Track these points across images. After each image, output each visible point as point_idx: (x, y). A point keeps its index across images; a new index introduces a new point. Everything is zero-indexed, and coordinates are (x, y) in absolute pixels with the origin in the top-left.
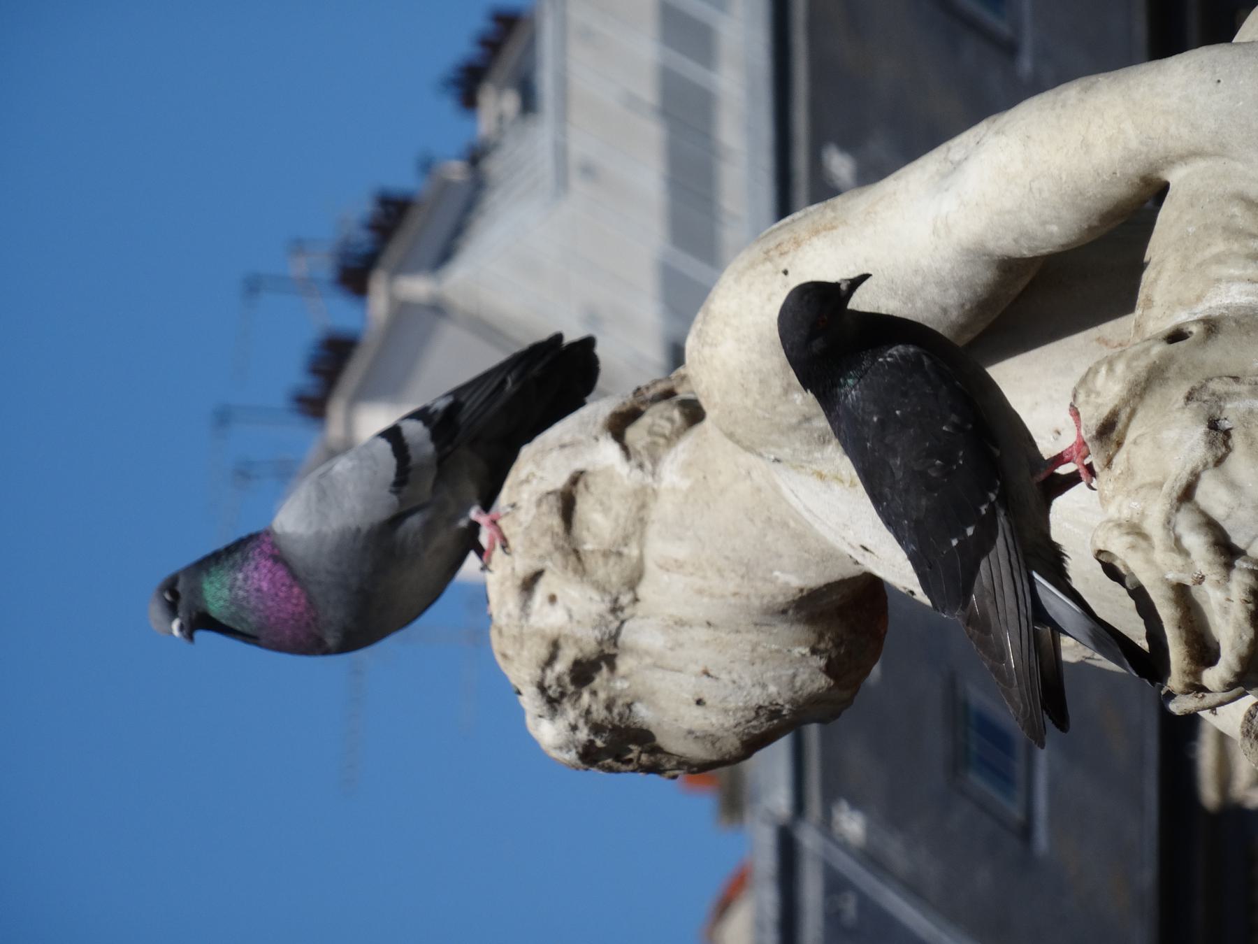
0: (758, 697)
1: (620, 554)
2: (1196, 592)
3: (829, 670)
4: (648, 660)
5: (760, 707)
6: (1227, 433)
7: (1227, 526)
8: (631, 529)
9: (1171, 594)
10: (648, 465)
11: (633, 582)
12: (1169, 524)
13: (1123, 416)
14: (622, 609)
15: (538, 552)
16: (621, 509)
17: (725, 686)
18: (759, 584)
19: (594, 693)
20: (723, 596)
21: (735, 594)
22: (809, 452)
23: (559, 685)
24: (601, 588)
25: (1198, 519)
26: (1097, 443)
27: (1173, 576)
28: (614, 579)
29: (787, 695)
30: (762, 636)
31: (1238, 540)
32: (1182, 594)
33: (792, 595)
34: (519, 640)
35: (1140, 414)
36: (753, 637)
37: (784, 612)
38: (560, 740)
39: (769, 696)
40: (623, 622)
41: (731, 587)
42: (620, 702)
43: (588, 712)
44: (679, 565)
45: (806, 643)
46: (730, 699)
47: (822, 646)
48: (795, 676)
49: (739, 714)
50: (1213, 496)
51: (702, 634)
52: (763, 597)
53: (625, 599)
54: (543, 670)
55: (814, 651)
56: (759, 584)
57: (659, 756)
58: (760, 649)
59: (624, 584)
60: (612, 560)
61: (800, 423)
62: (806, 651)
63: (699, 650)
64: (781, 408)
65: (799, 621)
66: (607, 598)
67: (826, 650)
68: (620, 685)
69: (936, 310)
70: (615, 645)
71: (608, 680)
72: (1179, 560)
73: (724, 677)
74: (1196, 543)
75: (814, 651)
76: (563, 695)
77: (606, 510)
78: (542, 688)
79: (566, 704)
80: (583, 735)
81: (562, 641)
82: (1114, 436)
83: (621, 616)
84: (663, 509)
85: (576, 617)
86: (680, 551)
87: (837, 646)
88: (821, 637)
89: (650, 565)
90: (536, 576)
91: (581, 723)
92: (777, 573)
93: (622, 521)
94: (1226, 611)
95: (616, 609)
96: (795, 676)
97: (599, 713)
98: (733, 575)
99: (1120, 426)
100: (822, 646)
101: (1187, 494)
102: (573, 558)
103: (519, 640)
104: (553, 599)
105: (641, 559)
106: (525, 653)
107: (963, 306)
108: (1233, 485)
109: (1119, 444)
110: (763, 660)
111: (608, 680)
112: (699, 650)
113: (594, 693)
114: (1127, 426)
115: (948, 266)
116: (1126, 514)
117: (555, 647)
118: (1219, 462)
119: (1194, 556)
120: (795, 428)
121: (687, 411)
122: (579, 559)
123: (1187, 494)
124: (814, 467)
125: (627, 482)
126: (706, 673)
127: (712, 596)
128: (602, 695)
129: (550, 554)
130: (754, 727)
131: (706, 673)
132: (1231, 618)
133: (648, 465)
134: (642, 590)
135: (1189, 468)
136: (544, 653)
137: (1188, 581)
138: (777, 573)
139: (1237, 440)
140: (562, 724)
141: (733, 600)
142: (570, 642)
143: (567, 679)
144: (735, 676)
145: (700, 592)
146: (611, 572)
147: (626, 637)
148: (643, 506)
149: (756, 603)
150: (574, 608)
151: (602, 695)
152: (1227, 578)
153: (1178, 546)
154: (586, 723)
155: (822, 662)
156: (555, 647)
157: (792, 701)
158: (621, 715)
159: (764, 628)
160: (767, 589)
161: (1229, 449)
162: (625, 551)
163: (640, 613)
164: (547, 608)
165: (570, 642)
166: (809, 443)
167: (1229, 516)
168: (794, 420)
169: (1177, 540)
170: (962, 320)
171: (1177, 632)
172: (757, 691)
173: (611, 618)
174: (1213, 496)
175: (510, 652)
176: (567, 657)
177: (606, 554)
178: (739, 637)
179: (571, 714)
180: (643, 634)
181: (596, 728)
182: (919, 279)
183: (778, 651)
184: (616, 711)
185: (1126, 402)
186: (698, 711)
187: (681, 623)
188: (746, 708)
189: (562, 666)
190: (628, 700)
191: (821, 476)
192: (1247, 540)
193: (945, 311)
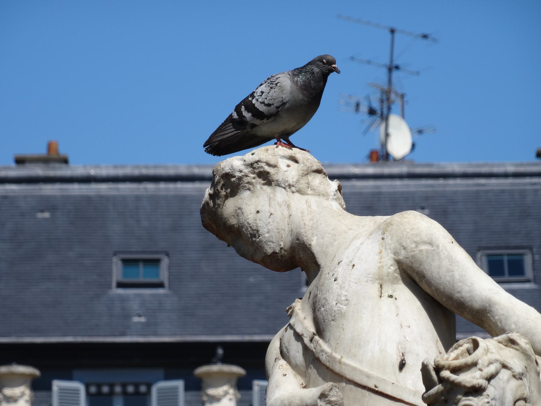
0: (263, 230)
1: (308, 188)
2: (474, 369)
3: (274, 253)
4: (272, 196)
5: (258, 231)
6: (521, 379)
7: (496, 378)
8: (317, 191)
9: (475, 361)
10: (335, 197)
11: (299, 191)
12: (497, 361)
13: (517, 347)
14: (290, 188)
15: (305, 161)
16: (322, 188)
17: (267, 220)
18: (310, 231)
19: (254, 178)
20: (303, 220)
21: (305, 224)
22: (390, 249)
23: (258, 167)
24: (298, 181)
25: (499, 369)
26: (507, 339)
27: (480, 362)
28: (301, 186)
29: (264, 240)
30: (287, 232)
31: (492, 382)
32: (474, 364)
33: (307, 242)
34: (274, 155)
35: (517, 352)
36: (287, 229)
37: (298, 239)
38: (235, 167)
39: (264, 234)
40: (285, 188)
41: (307, 223)
42: (250, 186)
43: (247, 176)
44: (310, 206)
45: (284, 246)
46: (261, 222)
47: (283, 251)
48: (273, 242)
49: (255, 225)
50: (504, 374)
51: (286, 213)
52: (305, 233)
53: (293, 189)
54: (265, 162)
55: (281, 248)
56: (310, 231)
57: (224, 198)
58: (283, 232)
59: (299, 189)
60: (307, 185)
61: (403, 246)
62: (282, 246)
63: (280, 213)
64: (408, 240)
65: (292, 244)
66: (294, 183)
67: (281, 252)
68: (258, 187)
69: (459, 290)
70: (276, 185)
71: (260, 183)
72: (486, 364)
73: (271, 220)
74: (492, 369)
75: (281, 248)
76: (254, 168)
77: (320, 183)
78: (257, 162)
79: (250, 169)
80: (238, 174)
81: (276, 168)
82: (509, 344)
83: (287, 188)
84: (325, 203)
85: (285, 173)
86: (314, 207)
87: (282, 256)
88: (285, 251)
89: (306, 197)
90: (296, 161)
91: (243, 174)
92: (316, 237)
93: (318, 188)
94: (474, 378)
95: (290, 186)
96: (273, 242)
97: (246, 180)
98: (312, 223)
99: (513, 346)
100: (283, 251)
101: (504, 366)
102: (306, 173)
103: (274, 155)
104: (288, 166)
105: (308, 194)
106: (271, 157)
107: (462, 298)
108: (508, 380)
109: (506, 346)
110: (279, 232)
111: (260, 183)
112: (280, 213)
113: (254, 178)
114: (513, 348)
115: (479, 294)
116: (490, 347)
117: (275, 166)
118: (514, 376)
119: (488, 368)
120: (401, 245)
121: (427, 211)
122: (306, 175)
123: (504, 366)
124: (384, 250)
125: (329, 190)
126: (271, 214)
127: (302, 217)
128: (253, 181)
129: (306, 165)
130: (247, 229)
131: (271, 214)
132: (472, 379)
133: (335, 197)
134: (297, 195)
135: (512, 367)
136: (272, 162)
137: (478, 366)
138: (316, 237)
139: (520, 382)
140: (242, 168)
141: (302, 223)
142: (277, 171)
143: (261, 170)
144: (272, 223)
145: (302, 213)
146: (302, 185)
147: (278, 189)
148: (324, 195)
149: (303, 230)
150: (288, 173)
151: (253, 181)
152: (483, 378)
153: (490, 363)
154: (243, 175)
155: (277, 251)
156: (275, 166)
157: (261, 241)
158: (245, 186)
159: (290, 233)
160: (309, 234)
161: (517, 379)
162: (309, 189)
163: (288, 193)
164: (286, 164)
165: (277, 171)
166: (394, 249)
167: (499, 379)
168: (404, 244)
169: (492, 363)
170: (455, 297)
171: (464, 363)
172: (266, 230)
173: (286, 184)
174: (504, 374)
175: (269, 152)
176: (271, 170)
177: (308, 183)
178: (286, 225)
179: (246, 171)
180: (280, 194)
181: (240, 179)
182: (470, 284)
183: (282, 237)
184: (247, 185)
185: (521, 348)
186: (254, 211)
187: (289, 206)
188: (257, 226)
189: (267, 168)
190: (252, 189)
191: (381, 252)
192: (493, 385)
193: (459, 292)
